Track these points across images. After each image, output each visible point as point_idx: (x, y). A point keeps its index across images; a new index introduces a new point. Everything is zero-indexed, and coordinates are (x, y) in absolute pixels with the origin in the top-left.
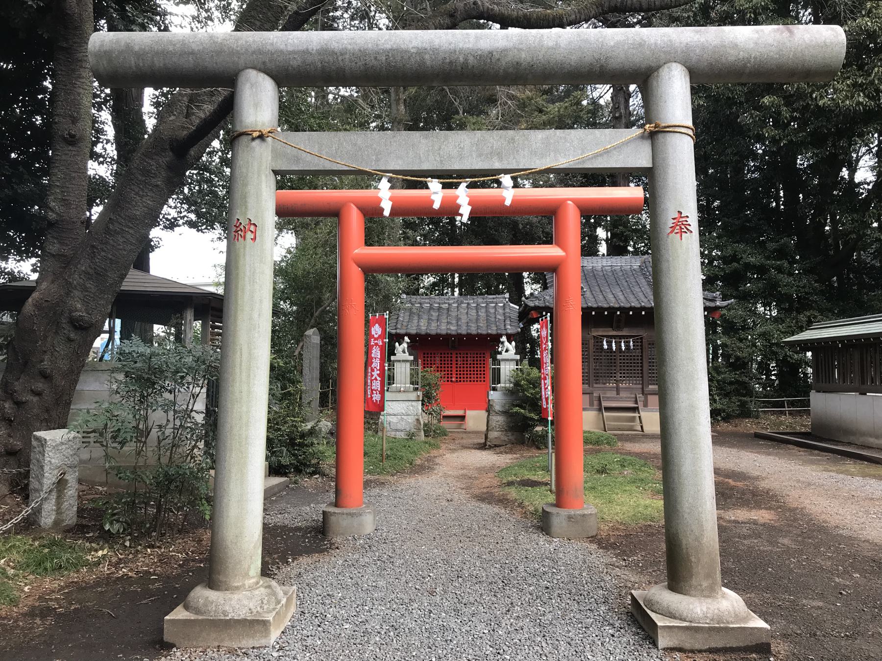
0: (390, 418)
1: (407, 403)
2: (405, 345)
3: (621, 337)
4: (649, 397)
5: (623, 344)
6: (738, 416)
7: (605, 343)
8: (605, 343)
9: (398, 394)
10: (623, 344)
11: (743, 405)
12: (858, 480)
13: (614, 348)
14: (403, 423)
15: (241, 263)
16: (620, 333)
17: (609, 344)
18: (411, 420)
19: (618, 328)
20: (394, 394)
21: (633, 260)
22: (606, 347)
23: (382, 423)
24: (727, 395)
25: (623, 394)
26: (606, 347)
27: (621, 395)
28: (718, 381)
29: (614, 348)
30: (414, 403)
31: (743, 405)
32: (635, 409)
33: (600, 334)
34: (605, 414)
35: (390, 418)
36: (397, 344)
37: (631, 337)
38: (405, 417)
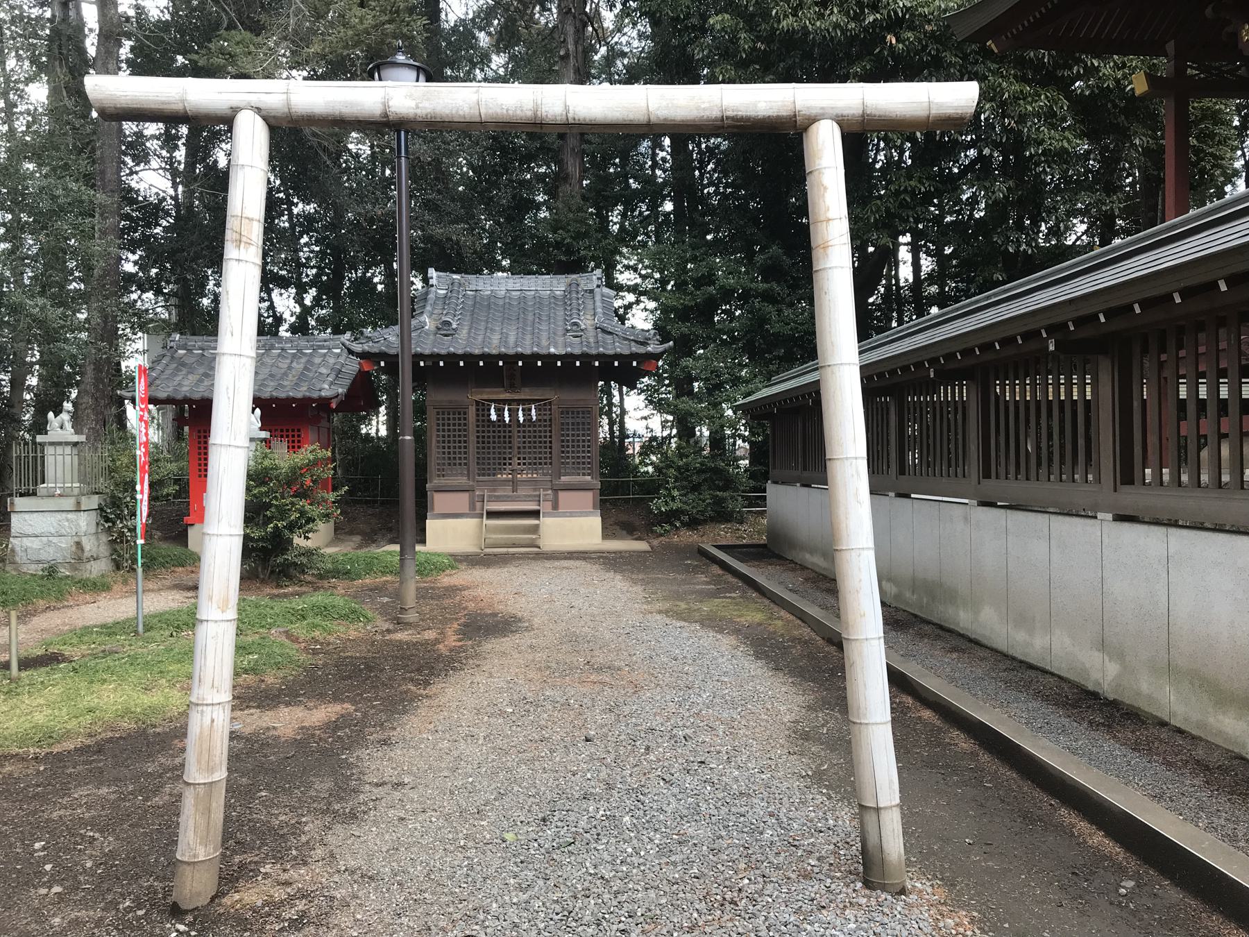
0: (27, 542)
1: (58, 516)
2: (65, 417)
3: (519, 402)
4: (562, 495)
5: (506, 414)
6: (712, 519)
7: (493, 411)
8: (493, 411)
9: (51, 500)
10: (506, 414)
11: (719, 502)
12: (210, 662)
13: (507, 419)
14: (51, 550)
15: (951, 111)
16: (502, 397)
17: (500, 412)
18: (66, 543)
19: (512, 387)
20: (46, 500)
21: (555, 282)
22: (494, 417)
23: (13, 550)
24: (695, 488)
25: (522, 491)
26: (494, 417)
27: (520, 492)
28: (678, 469)
29: (507, 419)
30: (70, 516)
31: (719, 502)
32: (535, 514)
33: (485, 397)
34: (485, 521)
35: (27, 542)
36: (51, 415)
37: (530, 401)
38: (55, 540)
